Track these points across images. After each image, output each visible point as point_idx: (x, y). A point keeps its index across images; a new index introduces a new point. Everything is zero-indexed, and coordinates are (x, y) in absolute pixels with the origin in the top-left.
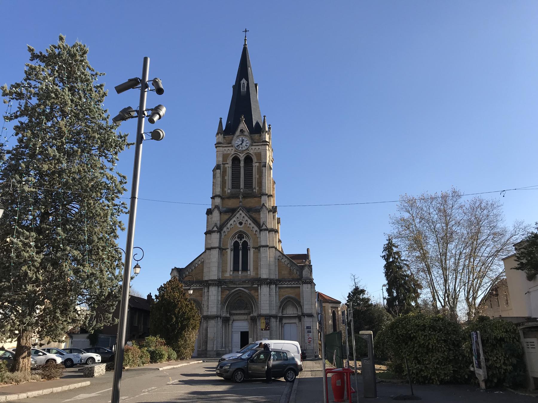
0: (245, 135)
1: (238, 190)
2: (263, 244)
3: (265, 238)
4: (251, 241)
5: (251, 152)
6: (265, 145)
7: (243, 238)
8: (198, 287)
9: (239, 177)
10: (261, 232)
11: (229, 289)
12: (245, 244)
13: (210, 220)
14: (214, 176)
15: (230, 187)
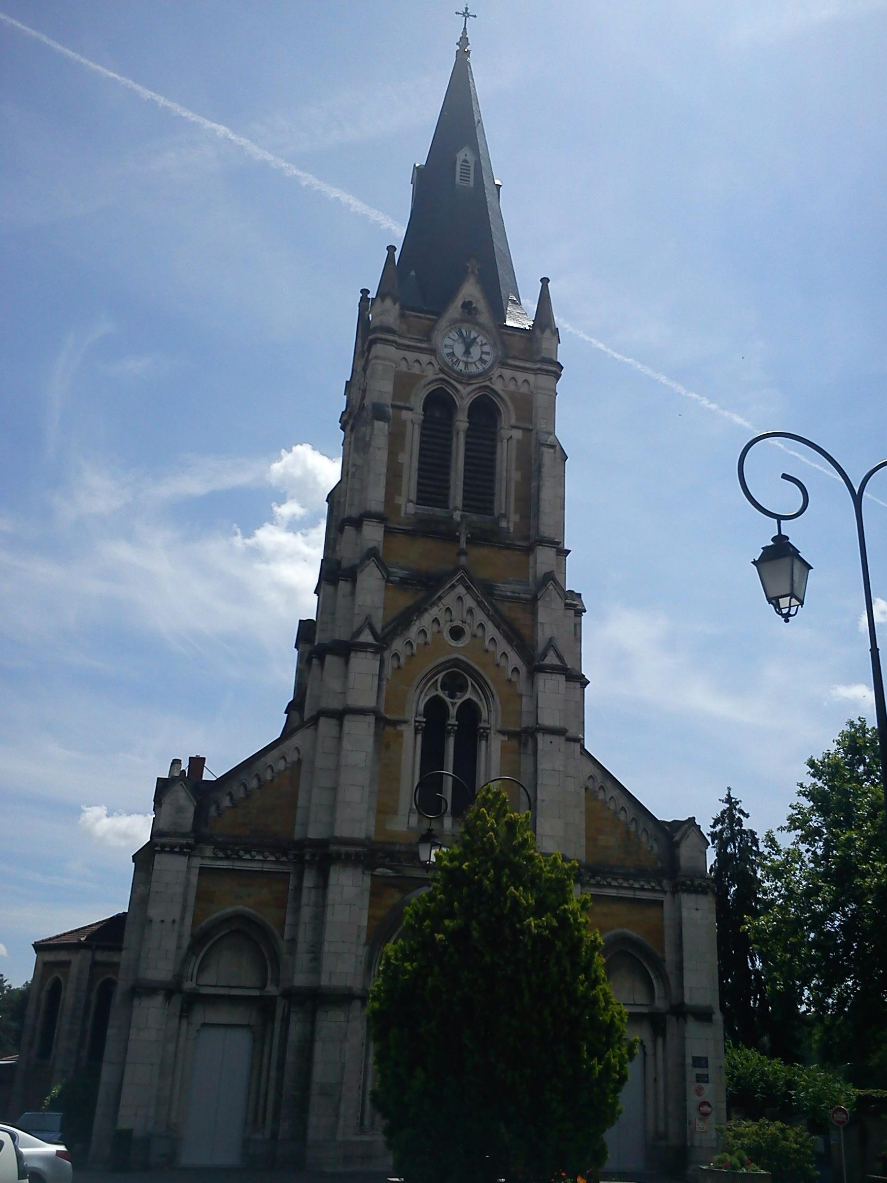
1: (439, 512)
5: (498, 386)
7: (463, 688)
8: (267, 867)
9: (445, 468)
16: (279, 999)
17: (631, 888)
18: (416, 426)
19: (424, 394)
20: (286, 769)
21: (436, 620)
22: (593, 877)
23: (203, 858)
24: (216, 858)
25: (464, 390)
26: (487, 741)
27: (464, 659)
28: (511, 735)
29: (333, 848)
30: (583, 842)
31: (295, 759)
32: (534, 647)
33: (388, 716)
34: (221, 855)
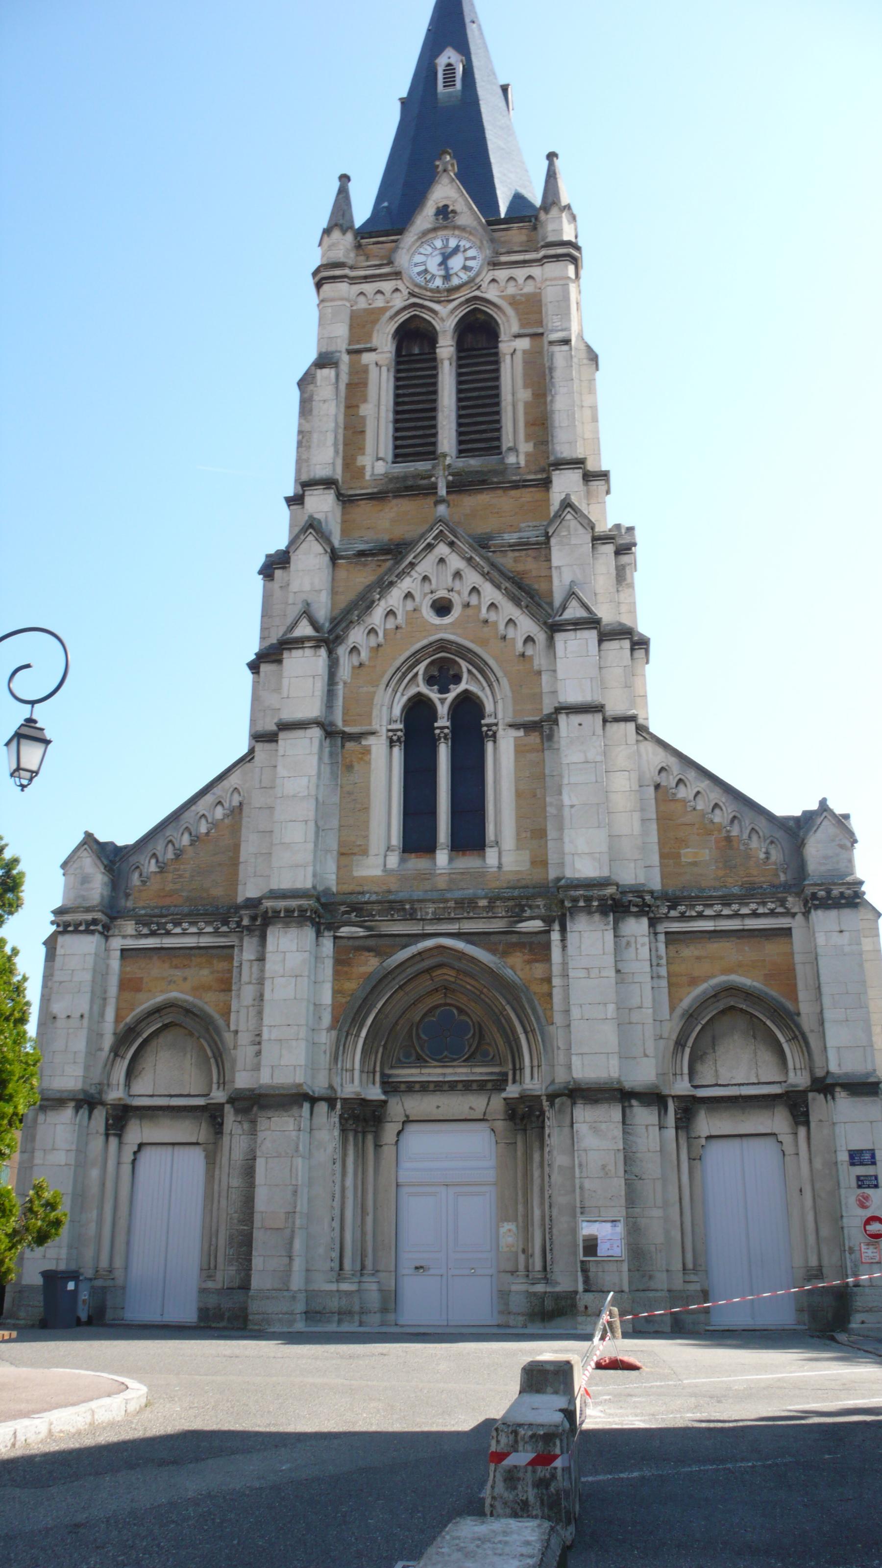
0: (462, 229)
2: (572, 695)
3: (575, 667)
4: (505, 688)
5: (492, 294)
6: (557, 257)
7: (457, 679)
8: (205, 941)
9: (431, 411)
10: (559, 637)
11: (382, 944)
12: (468, 710)
13: (278, 593)
14: (306, 407)
15: (386, 448)
16: (228, 1108)
17: (736, 915)
18: (384, 369)
19: (392, 327)
20: (226, 816)
21: (409, 595)
22: (673, 907)
23: (124, 937)
24: (140, 936)
25: (442, 310)
26: (495, 742)
27: (452, 637)
28: (529, 727)
29: (268, 904)
30: (655, 859)
31: (235, 803)
32: (551, 604)
33: (347, 729)
34: (145, 931)
